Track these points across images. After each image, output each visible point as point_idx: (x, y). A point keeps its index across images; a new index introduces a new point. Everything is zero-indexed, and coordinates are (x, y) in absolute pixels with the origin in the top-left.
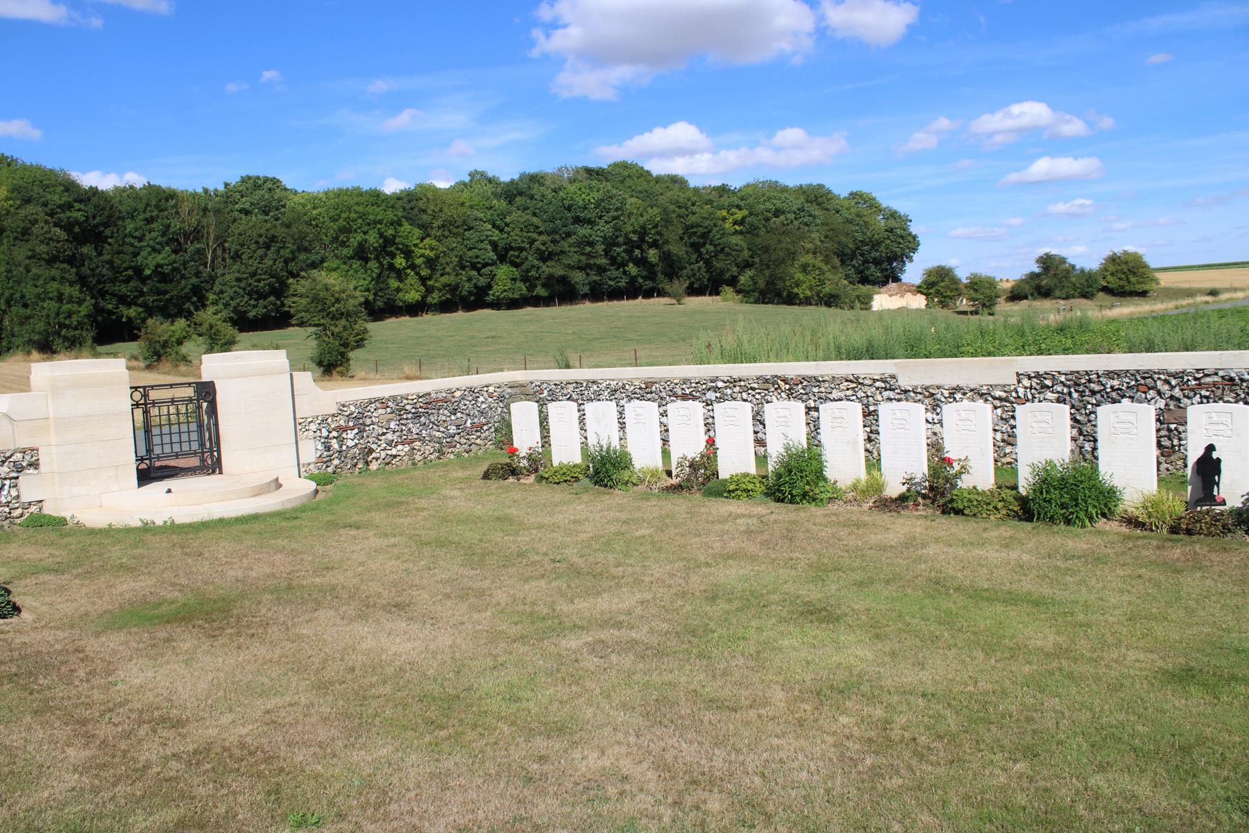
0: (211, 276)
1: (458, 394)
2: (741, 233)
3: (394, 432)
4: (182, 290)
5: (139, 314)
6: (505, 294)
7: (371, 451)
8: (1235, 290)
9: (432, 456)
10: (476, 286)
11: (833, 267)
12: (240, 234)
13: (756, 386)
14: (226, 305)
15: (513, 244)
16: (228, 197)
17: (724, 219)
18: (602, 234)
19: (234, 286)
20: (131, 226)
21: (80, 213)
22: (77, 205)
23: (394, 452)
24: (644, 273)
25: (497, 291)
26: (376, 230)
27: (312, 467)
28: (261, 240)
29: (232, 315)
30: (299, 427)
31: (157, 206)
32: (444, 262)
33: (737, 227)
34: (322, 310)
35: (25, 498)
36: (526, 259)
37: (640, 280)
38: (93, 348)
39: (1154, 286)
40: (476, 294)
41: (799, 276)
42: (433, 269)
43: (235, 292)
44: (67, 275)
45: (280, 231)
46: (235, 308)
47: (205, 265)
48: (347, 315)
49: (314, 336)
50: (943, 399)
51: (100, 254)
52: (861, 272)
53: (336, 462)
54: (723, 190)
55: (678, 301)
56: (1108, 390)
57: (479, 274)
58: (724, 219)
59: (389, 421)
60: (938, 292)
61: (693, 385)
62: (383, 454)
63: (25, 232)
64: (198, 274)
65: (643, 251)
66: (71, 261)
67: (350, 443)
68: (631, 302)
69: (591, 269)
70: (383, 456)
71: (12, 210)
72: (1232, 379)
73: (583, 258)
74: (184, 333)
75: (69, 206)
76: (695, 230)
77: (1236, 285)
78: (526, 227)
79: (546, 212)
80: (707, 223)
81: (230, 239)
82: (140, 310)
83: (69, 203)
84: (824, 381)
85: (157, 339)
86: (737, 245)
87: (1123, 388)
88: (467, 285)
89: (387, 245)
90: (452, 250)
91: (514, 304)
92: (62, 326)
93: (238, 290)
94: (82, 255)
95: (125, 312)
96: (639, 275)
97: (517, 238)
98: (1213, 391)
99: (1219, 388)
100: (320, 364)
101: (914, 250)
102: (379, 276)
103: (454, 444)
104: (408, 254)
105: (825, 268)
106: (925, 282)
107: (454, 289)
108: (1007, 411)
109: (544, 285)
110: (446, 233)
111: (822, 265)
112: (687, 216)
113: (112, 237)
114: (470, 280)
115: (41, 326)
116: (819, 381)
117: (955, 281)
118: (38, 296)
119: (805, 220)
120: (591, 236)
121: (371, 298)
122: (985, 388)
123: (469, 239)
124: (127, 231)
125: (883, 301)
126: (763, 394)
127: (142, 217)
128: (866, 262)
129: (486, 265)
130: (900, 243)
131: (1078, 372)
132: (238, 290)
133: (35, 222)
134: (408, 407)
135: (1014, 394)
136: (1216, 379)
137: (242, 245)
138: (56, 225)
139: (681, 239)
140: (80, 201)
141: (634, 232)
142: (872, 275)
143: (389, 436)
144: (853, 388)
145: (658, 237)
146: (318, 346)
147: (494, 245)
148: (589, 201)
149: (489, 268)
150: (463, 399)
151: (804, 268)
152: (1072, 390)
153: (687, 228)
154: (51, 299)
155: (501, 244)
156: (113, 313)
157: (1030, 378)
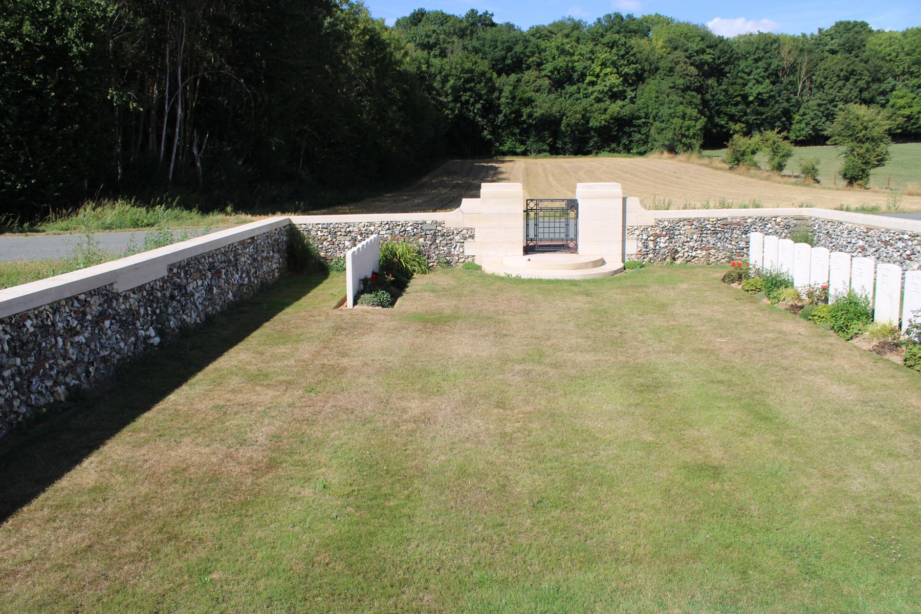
0: (797, 101)
1: (749, 221)
3: (696, 241)
4: (775, 112)
5: (742, 128)
7: (677, 252)
9: (723, 261)
12: (825, 69)
14: (807, 124)
16: (820, 40)
20: (744, 64)
21: (710, 56)
22: (708, 50)
23: (694, 254)
27: (633, 257)
28: (842, 74)
29: (811, 132)
30: (627, 232)
31: (764, 49)
35: (466, 254)
38: (700, 152)
43: (815, 114)
44: (694, 100)
45: (859, 67)
46: (813, 126)
48: (873, 140)
49: (844, 155)
51: (720, 84)
53: (651, 256)
59: (693, 234)
61: (892, 235)
62: (686, 254)
63: (671, 70)
66: (699, 90)
67: (662, 245)
70: (685, 256)
71: (665, 55)
74: (757, 146)
75: (703, 52)
81: (817, 73)
82: (744, 125)
83: (703, 49)
85: (738, 149)
92: (683, 136)
93: (818, 113)
94: (707, 85)
95: (733, 127)
100: (845, 176)
103: (742, 254)
113: (729, 72)
115: (670, 135)
118: (670, 115)
124: (741, 68)
127: (753, 57)
132: (818, 113)
133: (677, 63)
134: (708, 226)
138: (692, 64)
140: (710, 47)
143: (691, 244)
150: (754, 224)
154: (678, 117)
156: (725, 128)
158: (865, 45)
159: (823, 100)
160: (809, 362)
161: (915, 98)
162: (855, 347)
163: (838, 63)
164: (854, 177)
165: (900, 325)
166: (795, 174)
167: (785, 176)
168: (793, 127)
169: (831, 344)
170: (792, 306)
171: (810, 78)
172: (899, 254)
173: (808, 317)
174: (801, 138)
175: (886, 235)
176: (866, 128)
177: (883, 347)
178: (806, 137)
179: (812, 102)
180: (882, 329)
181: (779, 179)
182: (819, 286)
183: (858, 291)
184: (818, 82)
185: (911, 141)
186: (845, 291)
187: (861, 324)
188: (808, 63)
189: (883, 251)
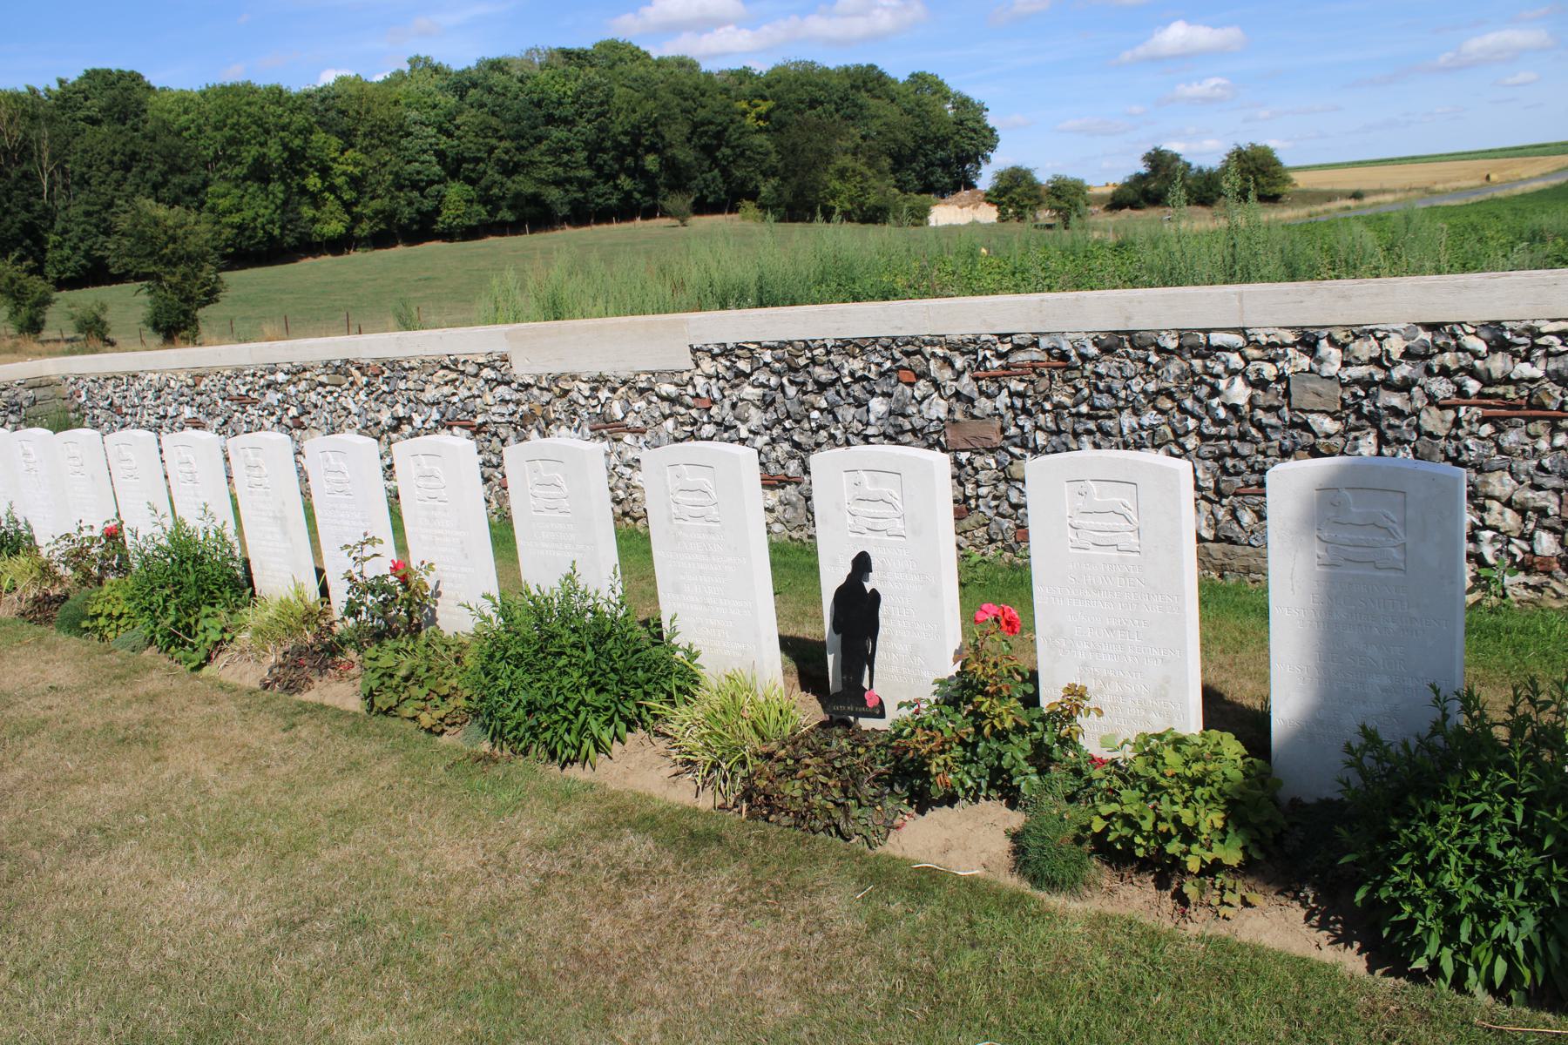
0: (46, 209)
2: (767, 130)
6: (458, 220)
8: (1383, 192)
10: (419, 211)
11: (880, 172)
12: (85, 151)
13: (324, 379)
14: (75, 249)
15: (466, 154)
16: (66, 100)
17: (744, 114)
18: (584, 138)
19: (84, 222)
24: (642, 187)
25: (447, 217)
26: (278, 140)
29: (84, 262)
32: (373, 181)
33: (761, 123)
34: (151, 254)
36: (485, 172)
37: (637, 196)
39: (1288, 188)
40: (420, 222)
41: (836, 184)
42: (361, 193)
43: (84, 231)
45: (144, 147)
46: (85, 251)
47: (39, 195)
48: (189, 258)
50: (582, 401)
52: (926, 177)
54: (744, 75)
55: (682, 221)
56: (847, 380)
57: (422, 195)
58: (744, 114)
60: (1012, 200)
61: (249, 379)
64: (28, 207)
65: (637, 158)
68: (625, 225)
69: (571, 184)
72: (1064, 356)
73: (560, 170)
76: (706, 128)
77: (1386, 186)
78: (482, 130)
79: (509, 110)
80: (719, 119)
81: (71, 158)
84: (412, 369)
86: (761, 146)
87: (872, 376)
88: (407, 211)
89: (296, 160)
90: (385, 165)
91: (471, 233)
93: (88, 227)
96: (635, 190)
97: (470, 145)
98: (1032, 382)
99: (1041, 375)
100: (156, 326)
101: (992, 148)
102: (285, 203)
104: (324, 172)
105: (869, 173)
106: (996, 189)
107: (389, 216)
108: (683, 424)
109: (510, 208)
110: (375, 142)
111: (864, 169)
112: (695, 110)
114: (410, 204)
116: (404, 369)
117: (1034, 186)
119: (848, 112)
120: (568, 140)
121: (277, 232)
122: (643, 377)
123: (406, 149)
125: (944, 214)
126: (336, 395)
128: (930, 164)
129: (431, 183)
130: (972, 139)
131: (790, 343)
132: (88, 227)
135: (690, 389)
136: (1035, 354)
137: (90, 167)
139: (689, 140)
141: (626, 133)
142: (938, 181)
144: (454, 381)
145: (656, 140)
146: (152, 302)
147: (441, 155)
148: (565, 93)
149: (436, 187)
151: (842, 174)
152: (785, 380)
153: (695, 126)
155: (451, 153)
157: (714, 357)
158: (145, 111)
159: (94, 204)
160: (84, 793)
161: (243, 196)
162: (222, 687)
163: (105, 140)
164: (172, 327)
165: (324, 591)
166: (67, 336)
167: (48, 341)
168: (49, 255)
169: (152, 699)
170: (36, 600)
171: (60, 167)
172: (274, 419)
173: (77, 625)
174: (68, 274)
175: (238, 382)
176: (173, 239)
177: (298, 666)
178: (77, 272)
179: (73, 210)
180: (281, 614)
181: (37, 347)
182: (97, 533)
183: (193, 521)
184: (76, 173)
185: (252, 266)
186: (159, 529)
187: (223, 613)
188: (51, 141)
189: (239, 421)
